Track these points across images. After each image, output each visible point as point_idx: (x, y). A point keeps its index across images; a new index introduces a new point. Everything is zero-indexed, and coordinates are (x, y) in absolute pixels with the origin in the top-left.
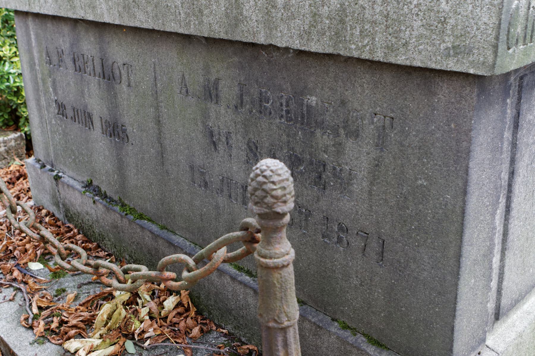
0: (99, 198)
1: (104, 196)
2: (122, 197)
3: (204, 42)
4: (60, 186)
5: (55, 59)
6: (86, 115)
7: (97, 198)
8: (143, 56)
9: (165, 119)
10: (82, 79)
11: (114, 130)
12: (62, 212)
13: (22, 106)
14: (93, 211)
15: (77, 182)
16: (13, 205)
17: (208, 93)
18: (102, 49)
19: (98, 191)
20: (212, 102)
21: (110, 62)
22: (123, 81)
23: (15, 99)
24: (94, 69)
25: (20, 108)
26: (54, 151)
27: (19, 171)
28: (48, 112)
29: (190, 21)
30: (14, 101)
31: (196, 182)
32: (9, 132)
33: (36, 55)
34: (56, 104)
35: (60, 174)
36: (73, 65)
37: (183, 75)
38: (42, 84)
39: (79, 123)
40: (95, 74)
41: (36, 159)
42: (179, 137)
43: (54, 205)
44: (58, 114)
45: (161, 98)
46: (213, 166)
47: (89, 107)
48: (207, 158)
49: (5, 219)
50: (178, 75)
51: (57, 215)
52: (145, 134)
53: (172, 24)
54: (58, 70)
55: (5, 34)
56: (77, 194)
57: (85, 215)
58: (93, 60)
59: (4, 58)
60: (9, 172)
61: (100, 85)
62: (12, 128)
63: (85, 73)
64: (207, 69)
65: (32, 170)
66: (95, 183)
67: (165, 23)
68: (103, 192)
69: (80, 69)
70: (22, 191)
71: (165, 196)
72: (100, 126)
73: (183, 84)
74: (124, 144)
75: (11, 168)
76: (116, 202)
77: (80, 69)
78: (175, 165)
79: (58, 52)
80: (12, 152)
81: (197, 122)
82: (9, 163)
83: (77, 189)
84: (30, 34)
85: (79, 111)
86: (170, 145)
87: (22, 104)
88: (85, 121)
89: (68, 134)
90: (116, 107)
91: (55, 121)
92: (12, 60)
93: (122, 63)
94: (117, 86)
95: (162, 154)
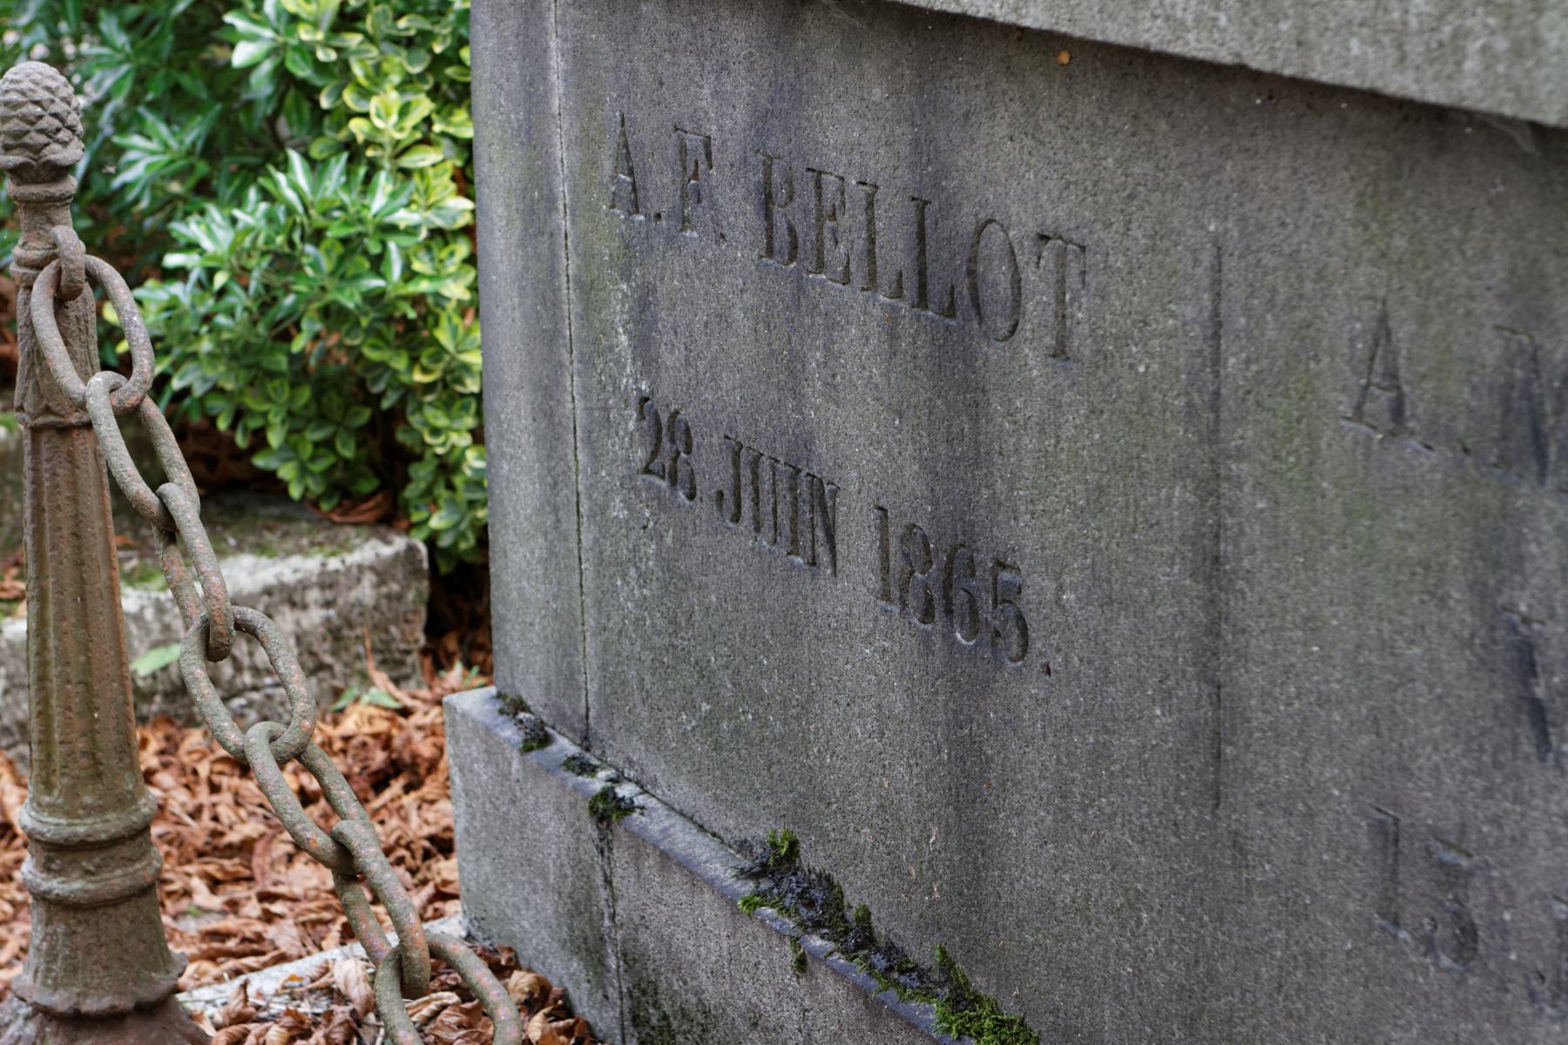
0: (831, 945)
1: (859, 937)
2: (957, 955)
3: (1527, 145)
4: (620, 855)
5: (662, 183)
6: (803, 488)
7: (816, 942)
8: (1155, 198)
9: (1252, 551)
10: (797, 299)
11: (947, 586)
12: (613, 994)
13: (429, 398)
14: (790, 1012)
15: (714, 843)
16: (415, 955)
17: (1522, 430)
18: (923, 151)
19: (826, 905)
20: (1542, 476)
21: (966, 221)
22: (1026, 328)
23: (400, 363)
24: (871, 253)
25: (420, 407)
26: (603, 667)
27: (386, 742)
28: (595, 457)
29: (1460, 35)
30: (395, 372)
31: (1406, 917)
32: (351, 532)
33: (562, 152)
34: (641, 417)
35: (625, 791)
36: (758, 223)
37: (1383, 319)
38: (576, 308)
39: (757, 530)
40: (872, 276)
41: (500, 696)
42: (1325, 659)
43: (576, 952)
44: (647, 471)
45: (1241, 435)
46: (1520, 840)
47: (821, 447)
48: (1488, 792)
49: (323, 1005)
50: (1351, 318)
51: (586, 1009)
52: (1124, 624)
53: (1354, 44)
54: (670, 239)
55: (386, 28)
56: (710, 909)
57: (743, 1027)
58: (870, 205)
59: (370, 153)
60: (338, 745)
61: (893, 336)
62: (367, 511)
63: (821, 266)
64: (1527, 296)
65: (475, 750)
66: (813, 859)
67: (1312, 35)
68: (851, 915)
69: (794, 246)
70: (402, 852)
71: (1211, 976)
72: (873, 556)
73: (1378, 367)
74: (999, 666)
75: (349, 725)
76: (922, 975)
77: (794, 246)
78: (1287, 812)
79: (683, 150)
80: (360, 639)
81: (1441, 582)
82: (337, 693)
83: (711, 883)
84: (546, 50)
85: (765, 462)
86: (1266, 694)
87: (429, 388)
88: (793, 521)
89: (688, 579)
90: (977, 464)
91: (628, 505)
92: (407, 161)
93: (1032, 227)
94: (993, 352)
95: (1215, 739)
